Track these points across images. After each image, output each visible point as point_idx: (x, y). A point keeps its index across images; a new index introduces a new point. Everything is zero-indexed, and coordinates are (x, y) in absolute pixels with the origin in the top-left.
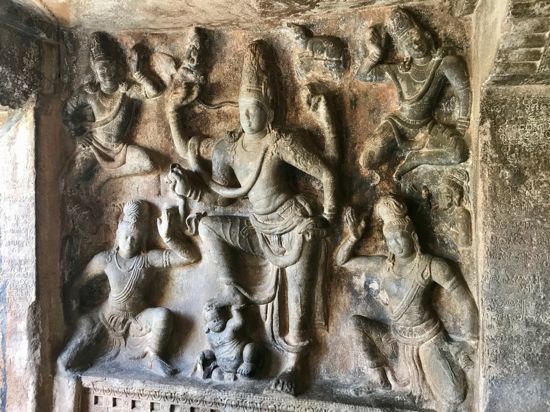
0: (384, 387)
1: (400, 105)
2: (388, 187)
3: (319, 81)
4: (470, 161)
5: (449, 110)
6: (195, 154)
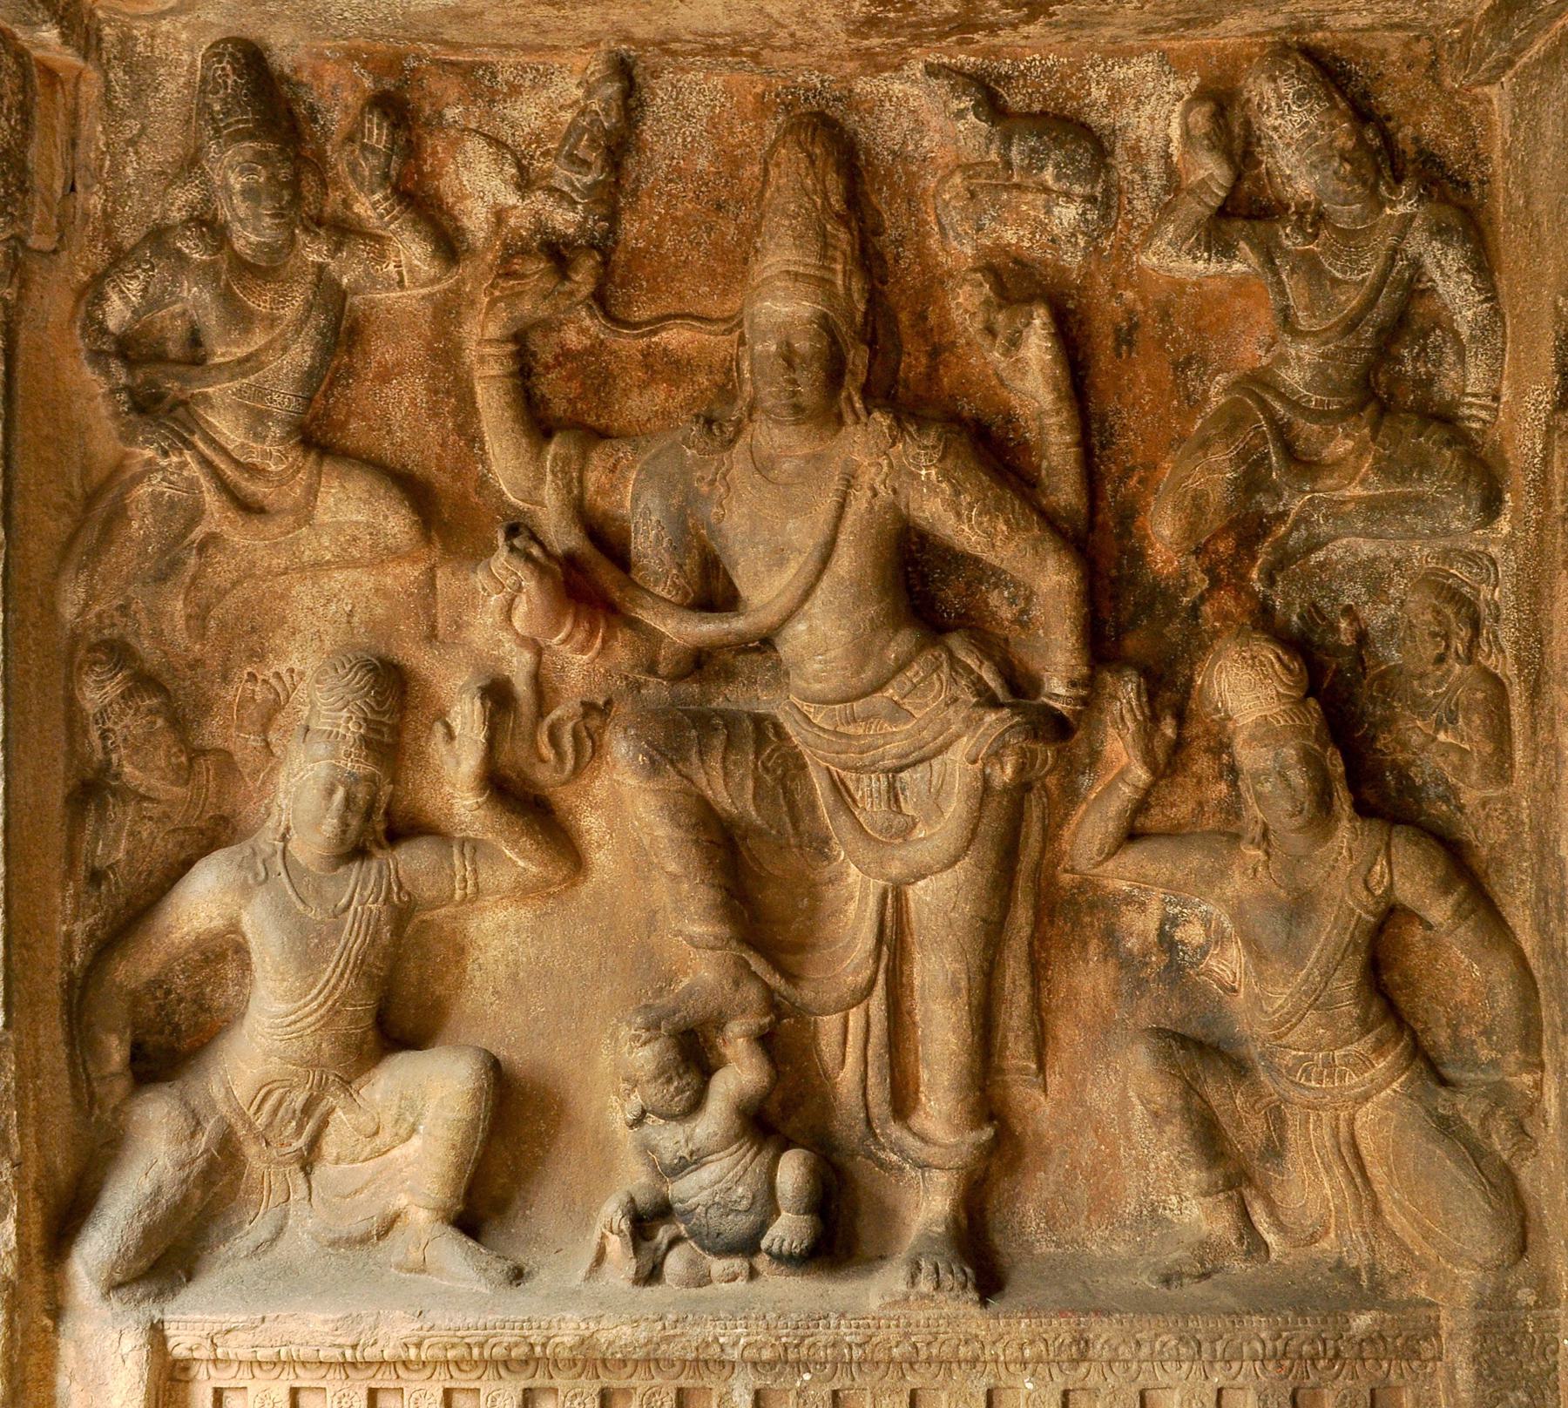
0: (1248, 1252)
1: (1268, 351)
2: (1236, 611)
3: (1016, 261)
4: (1504, 526)
5: (1423, 370)
6: (570, 492)
